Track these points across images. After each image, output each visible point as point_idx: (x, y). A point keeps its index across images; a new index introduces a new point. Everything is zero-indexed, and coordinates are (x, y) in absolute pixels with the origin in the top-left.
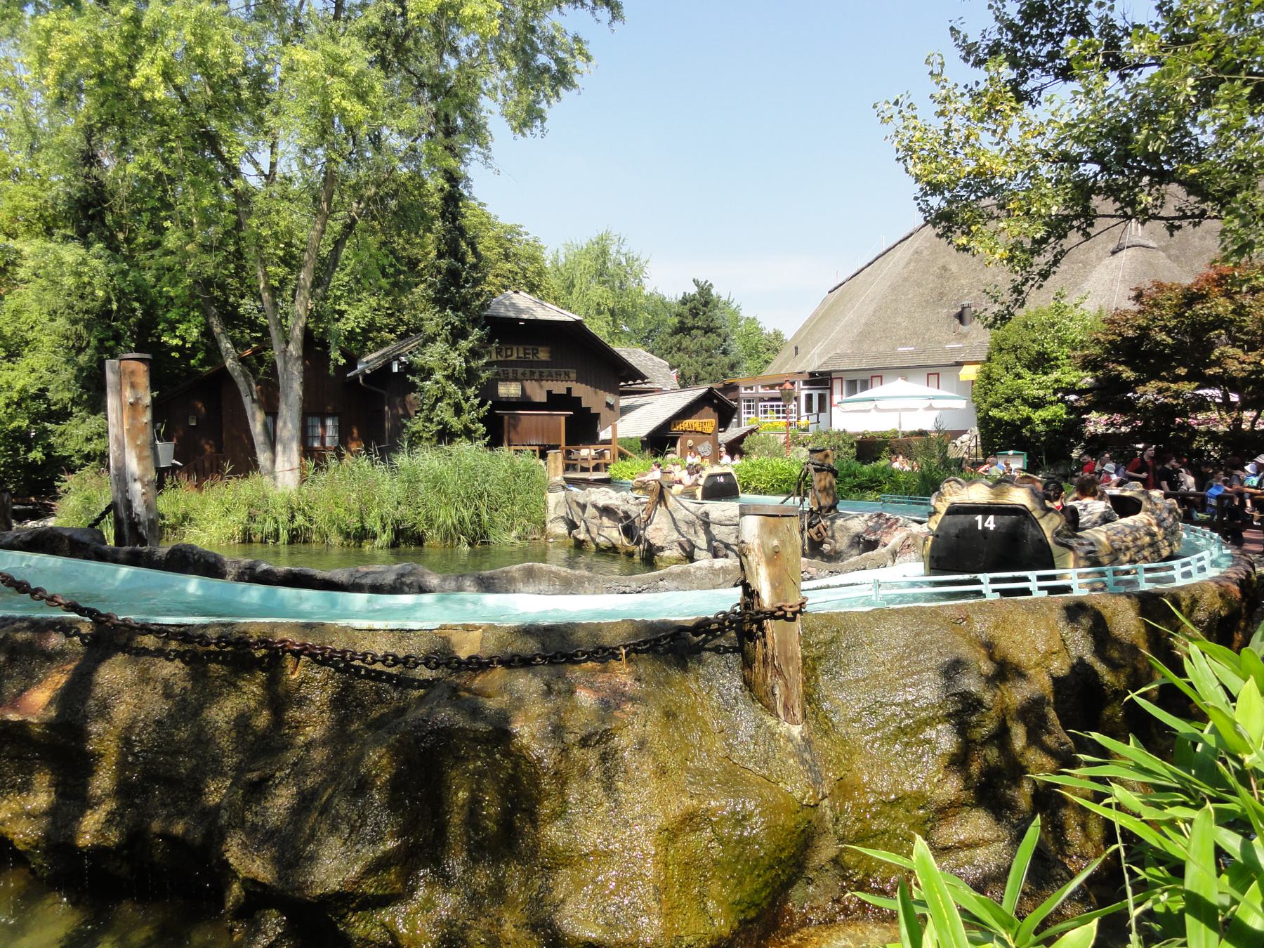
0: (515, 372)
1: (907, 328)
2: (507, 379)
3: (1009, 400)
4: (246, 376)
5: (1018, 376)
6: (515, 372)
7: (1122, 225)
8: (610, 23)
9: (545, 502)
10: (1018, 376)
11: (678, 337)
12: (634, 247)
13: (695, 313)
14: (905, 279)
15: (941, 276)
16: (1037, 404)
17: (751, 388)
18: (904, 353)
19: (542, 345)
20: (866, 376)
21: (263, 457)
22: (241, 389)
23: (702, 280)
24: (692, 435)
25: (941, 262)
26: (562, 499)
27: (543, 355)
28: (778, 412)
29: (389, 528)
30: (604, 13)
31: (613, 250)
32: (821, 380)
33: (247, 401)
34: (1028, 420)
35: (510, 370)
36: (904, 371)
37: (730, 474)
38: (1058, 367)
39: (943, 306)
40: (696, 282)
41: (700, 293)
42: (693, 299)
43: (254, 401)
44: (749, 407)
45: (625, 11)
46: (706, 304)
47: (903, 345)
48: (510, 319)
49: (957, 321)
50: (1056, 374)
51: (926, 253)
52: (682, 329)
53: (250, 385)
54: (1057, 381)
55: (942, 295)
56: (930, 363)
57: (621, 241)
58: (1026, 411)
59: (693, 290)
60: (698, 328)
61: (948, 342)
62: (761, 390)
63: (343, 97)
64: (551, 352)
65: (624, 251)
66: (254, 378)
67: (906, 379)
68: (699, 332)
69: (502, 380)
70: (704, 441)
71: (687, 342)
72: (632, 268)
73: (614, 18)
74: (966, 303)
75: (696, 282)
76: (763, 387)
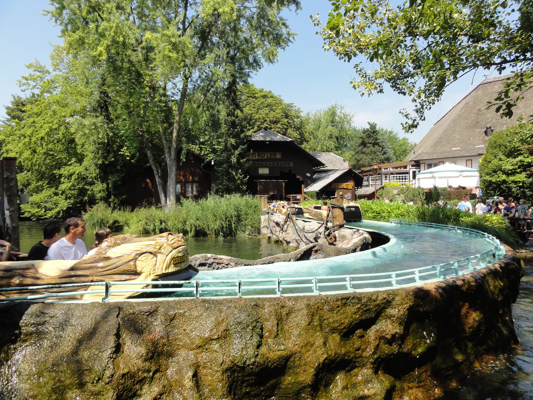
0: (266, 164)
1: (458, 139)
2: (262, 167)
3: (495, 172)
4: (156, 167)
5: (500, 160)
6: (266, 164)
7: (474, 70)
8: (296, 11)
9: (260, 219)
10: (500, 160)
11: (361, 147)
12: (347, 110)
13: (369, 136)
14: (460, 116)
15: (477, 114)
16: (513, 173)
17: (387, 169)
18: (454, 151)
19: (277, 152)
20: (436, 162)
21: (163, 201)
22: (155, 173)
23: (372, 122)
24: (342, 190)
25: (478, 108)
26: (267, 218)
27: (278, 156)
28: (397, 179)
29: (193, 229)
30: (293, 7)
31: (338, 112)
32: (417, 164)
33: (157, 177)
34: (504, 182)
35: (264, 163)
36: (454, 159)
37: (301, 209)
38: (522, 154)
39: (477, 128)
40: (369, 123)
41: (370, 128)
42: (368, 130)
43: (159, 177)
44: (386, 177)
45: (302, 5)
46: (374, 132)
47: (456, 147)
48: (261, 141)
49: (484, 135)
50: (520, 158)
51: (471, 103)
52: (364, 144)
53: (158, 171)
54: (521, 161)
55: (477, 122)
56: (467, 155)
57: (342, 108)
58: (504, 177)
59: (368, 127)
60: (370, 143)
61: (479, 144)
62: (391, 170)
63: (170, 51)
64: (282, 155)
65: (343, 112)
66: (160, 167)
67: (455, 163)
68: (371, 145)
69: (260, 167)
70: (347, 193)
71: (365, 150)
72: (346, 119)
73: (297, 8)
74: (488, 126)
75: (369, 123)
76: (392, 168)
